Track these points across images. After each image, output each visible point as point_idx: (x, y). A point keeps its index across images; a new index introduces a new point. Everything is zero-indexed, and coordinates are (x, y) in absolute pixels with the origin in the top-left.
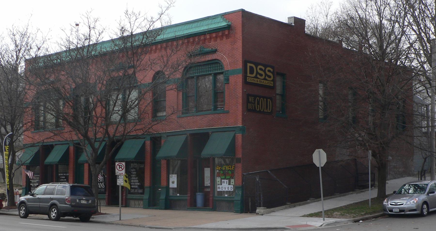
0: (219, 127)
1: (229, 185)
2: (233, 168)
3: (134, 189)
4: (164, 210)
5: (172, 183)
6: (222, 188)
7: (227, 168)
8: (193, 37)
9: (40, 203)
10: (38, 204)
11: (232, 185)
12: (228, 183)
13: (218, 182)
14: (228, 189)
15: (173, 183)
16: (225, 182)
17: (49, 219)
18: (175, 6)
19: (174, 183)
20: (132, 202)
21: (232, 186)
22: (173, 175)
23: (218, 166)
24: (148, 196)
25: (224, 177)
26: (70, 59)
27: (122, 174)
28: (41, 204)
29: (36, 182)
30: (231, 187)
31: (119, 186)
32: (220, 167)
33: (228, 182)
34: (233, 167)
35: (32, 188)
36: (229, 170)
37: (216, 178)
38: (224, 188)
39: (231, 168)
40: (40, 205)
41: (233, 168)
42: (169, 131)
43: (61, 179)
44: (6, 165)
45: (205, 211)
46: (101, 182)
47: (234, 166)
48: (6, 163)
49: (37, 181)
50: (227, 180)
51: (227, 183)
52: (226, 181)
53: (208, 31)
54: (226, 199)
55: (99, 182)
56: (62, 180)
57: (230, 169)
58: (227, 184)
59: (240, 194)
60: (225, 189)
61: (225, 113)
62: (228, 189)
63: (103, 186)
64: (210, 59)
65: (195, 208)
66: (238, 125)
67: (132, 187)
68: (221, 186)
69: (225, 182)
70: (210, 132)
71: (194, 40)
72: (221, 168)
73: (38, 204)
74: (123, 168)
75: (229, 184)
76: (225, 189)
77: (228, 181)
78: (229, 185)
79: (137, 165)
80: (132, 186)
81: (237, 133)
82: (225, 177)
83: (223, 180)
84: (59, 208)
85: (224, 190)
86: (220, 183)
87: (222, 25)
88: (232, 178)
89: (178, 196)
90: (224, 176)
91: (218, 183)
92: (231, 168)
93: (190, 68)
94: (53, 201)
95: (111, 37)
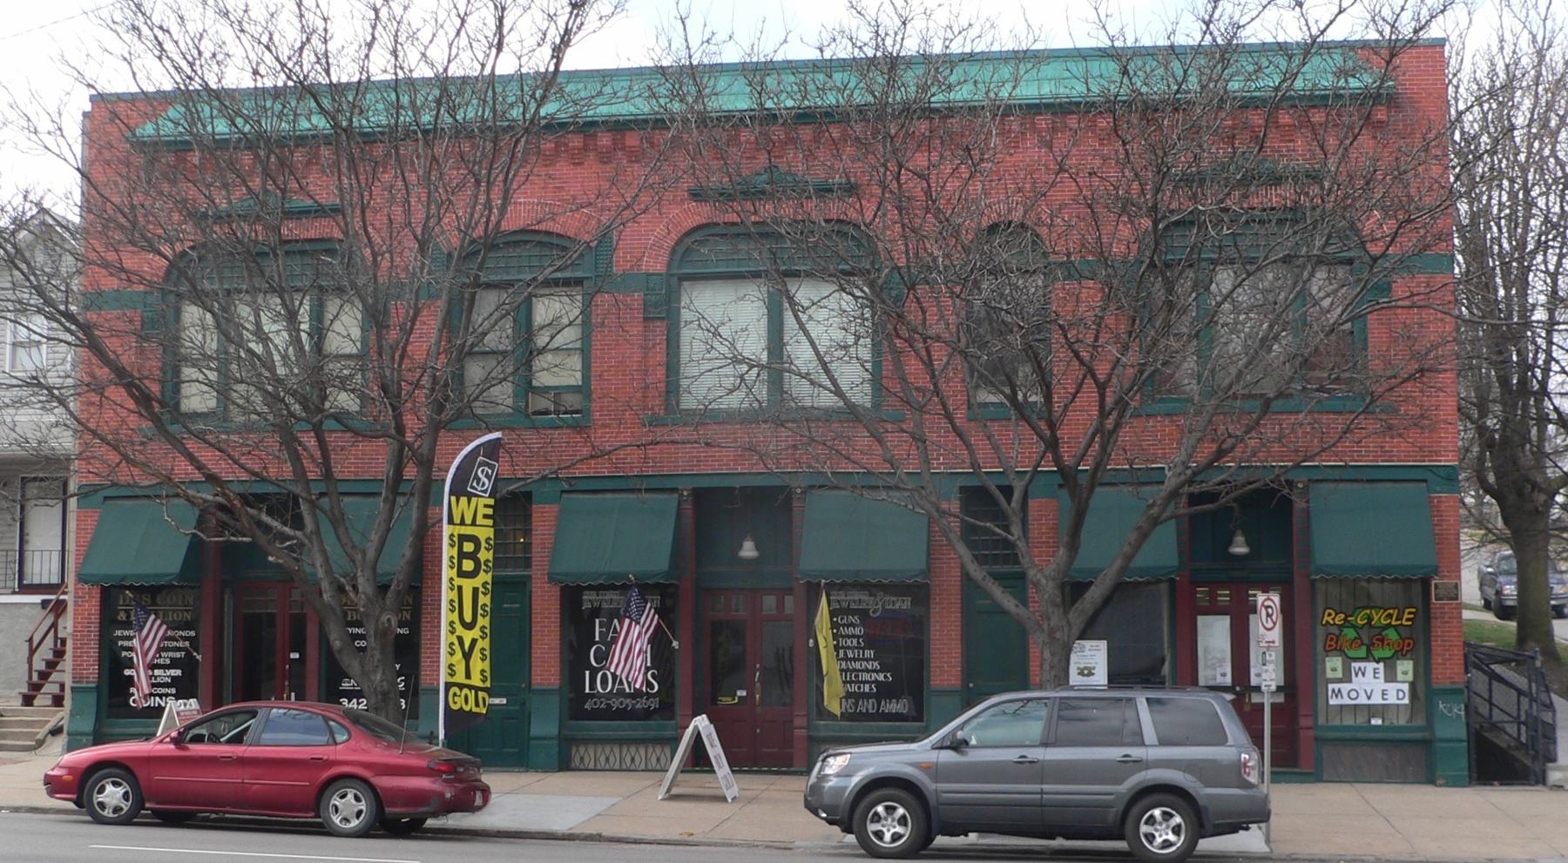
0: (1443, 464)
1: (1387, 681)
2: (1408, 620)
4: (553, 771)
6: (1353, 695)
7: (1376, 618)
9: (1042, 783)
10: (1037, 787)
13: (1334, 670)
14: (1383, 699)
16: (1369, 673)
18: (247, 6)
20: (588, 754)
22: (1088, 644)
23: (1328, 611)
24: (94, 720)
27: (1273, 642)
28: (1046, 787)
29: (168, 662)
30: (1398, 691)
31: (909, 695)
34: (1406, 616)
36: (1389, 626)
37: (1319, 658)
38: (1362, 694)
40: (1042, 792)
41: (1408, 620)
45: (1290, 782)
47: (1410, 613)
49: (173, 678)
50: (1378, 662)
52: (1370, 666)
59: (1459, 716)
60: (1369, 698)
61: (380, 437)
62: (1398, 699)
64: (312, 234)
65: (1285, 773)
66: (1440, 461)
68: (1345, 687)
69: (1369, 673)
70: (798, 485)
72: (1345, 619)
73: (1037, 787)
74: (1274, 617)
76: (1369, 698)
78: (1387, 681)
81: (1438, 488)
82: (1369, 651)
83: (1355, 665)
84: (932, 801)
86: (1339, 674)
88: (1404, 657)
91: (1330, 674)
94: (1149, 772)
95: (89, 86)
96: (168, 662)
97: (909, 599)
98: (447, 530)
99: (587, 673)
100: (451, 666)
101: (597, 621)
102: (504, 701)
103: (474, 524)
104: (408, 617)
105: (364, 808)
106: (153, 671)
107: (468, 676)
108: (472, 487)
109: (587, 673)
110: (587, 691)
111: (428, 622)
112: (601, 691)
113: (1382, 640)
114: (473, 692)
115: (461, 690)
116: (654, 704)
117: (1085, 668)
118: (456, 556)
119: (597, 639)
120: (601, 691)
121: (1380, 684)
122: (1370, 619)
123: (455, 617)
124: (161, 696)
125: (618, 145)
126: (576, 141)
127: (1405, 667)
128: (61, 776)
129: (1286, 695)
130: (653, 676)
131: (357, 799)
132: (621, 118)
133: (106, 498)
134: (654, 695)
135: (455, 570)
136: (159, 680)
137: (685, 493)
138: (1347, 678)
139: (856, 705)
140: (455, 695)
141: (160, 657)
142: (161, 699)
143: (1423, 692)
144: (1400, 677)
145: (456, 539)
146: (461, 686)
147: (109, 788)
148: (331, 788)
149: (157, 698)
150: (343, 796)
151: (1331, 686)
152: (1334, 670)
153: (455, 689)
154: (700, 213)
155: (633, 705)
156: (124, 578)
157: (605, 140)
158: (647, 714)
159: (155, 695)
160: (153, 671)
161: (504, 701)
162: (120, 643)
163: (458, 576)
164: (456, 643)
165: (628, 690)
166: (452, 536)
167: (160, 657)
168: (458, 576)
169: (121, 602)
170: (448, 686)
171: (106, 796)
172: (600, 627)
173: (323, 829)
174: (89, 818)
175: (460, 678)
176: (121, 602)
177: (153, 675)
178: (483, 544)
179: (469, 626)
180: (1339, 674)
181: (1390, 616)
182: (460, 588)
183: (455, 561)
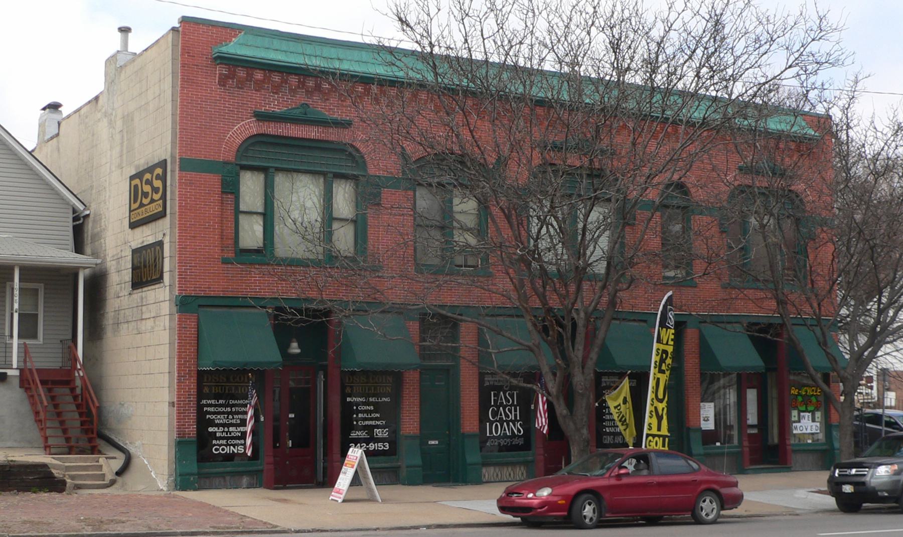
3: (612, 437)
4: (412, 482)
5: (704, 420)
6: (801, 428)
8: (281, 72)
11: (818, 422)
12: (810, 419)
13: (795, 416)
15: (795, 416)
17: (693, 521)
19: (708, 420)
21: (818, 424)
22: (707, 404)
25: (803, 408)
26: (665, 88)
29: (239, 422)
32: (797, 390)
33: (810, 417)
35: (214, 442)
36: (813, 395)
39: (816, 392)
42: (703, 312)
43: (358, 412)
44: (655, 368)
46: (511, 420)
48: (656, 362)
51: (808, 418)
52: (807, 414)
53: (362, 77)
54: (811, 448)
55: (505, 421)
56: (360, 415)
57: (815, 394)
58: (809, 420)
60: (806, 429)
63: (519, 431)
67: (608, 431)
68: (798, 425)
71: (250, 77)
72: (798, 392)
75: (813, 421)
76: (806, 429)
77: (810, 414)
79: (617, 380)
80: (607, 429)
82: (806, 408)
83: (802, 414)
85: (804, 431)
86: (796, 419)
87: (290, 60)
88: (818, 410)
89: (718, 447)
90: (804, 406)
92: (816, 392)
93: (343, 151)
96: (239, 422)
97: (635, 380)
98: (655, 345)
99: (488, 424)
100: (650, 425)
101: (492, 393)
102: (437, 442)
103: (667, 344)
104: (390, 391)
105: (715, 507)
106: (228, 428)
107: (659, 429)
108: (669, 323)
109: (488, 424)
110: (488, 435)
111: (407, 394)
112: (495, 434)
113: (810, 402)
114: (661, 439)
115: (654, 438)
116: (521, 442)
117: (706, 417)
118: (658, 361)
119: (492, 404)
120: (495, 434)
121: (810, 423)
122: (806, 392)
123: (654, 396)
124: (234, 446)
125: (334, 89)
126: (242, 73)
127: (818, 414)
128: (556, 502)
129: (758, 429)
130: (520, 424)
131: (711, 502)
132: (318, 68)
133: (200, 306)
134: (519, 437)
135: (657, 369)
136: (233, 434)
137: (540, 319)
138: (799, 421)
139: (614, 439)
140: (650, 441)
141: (233, 418)
142: (234, 447)
143: (828, 426)
144: (817, 420)
145: (660, 352)
146: (654, 436)
147: (703, 505)
148: (714, 495)
149: (232, 447)
150: (704, 501)
151: (794, 424)
152: (818, 418)
153: (650, 438)
154: (253, 128)
155: (512, 442)
156: (246, 364)
157: (374, 88)
158: (517, 448)
159: (230, 445)
160: (228, 428)
161: (437, 442)
162: (205, 409)
163: (659, 372)
164: (654, 410)
165: (508, 434)
166: (658, 349)
167: (233, 418)
168: (659, 372)
169: (205, 380)
170: (648, 435)
171: (587, 512)
172: (494, 397)
173: (698, 521)
174: (693, 521)
175: (654, 431)
176: (205, 380)
177: (228, 431)
178: (669, 355)
179: (661, 401)
180: (796, 419)
181: (813, 390)
182: (658, 379)
183: (658, 364)
